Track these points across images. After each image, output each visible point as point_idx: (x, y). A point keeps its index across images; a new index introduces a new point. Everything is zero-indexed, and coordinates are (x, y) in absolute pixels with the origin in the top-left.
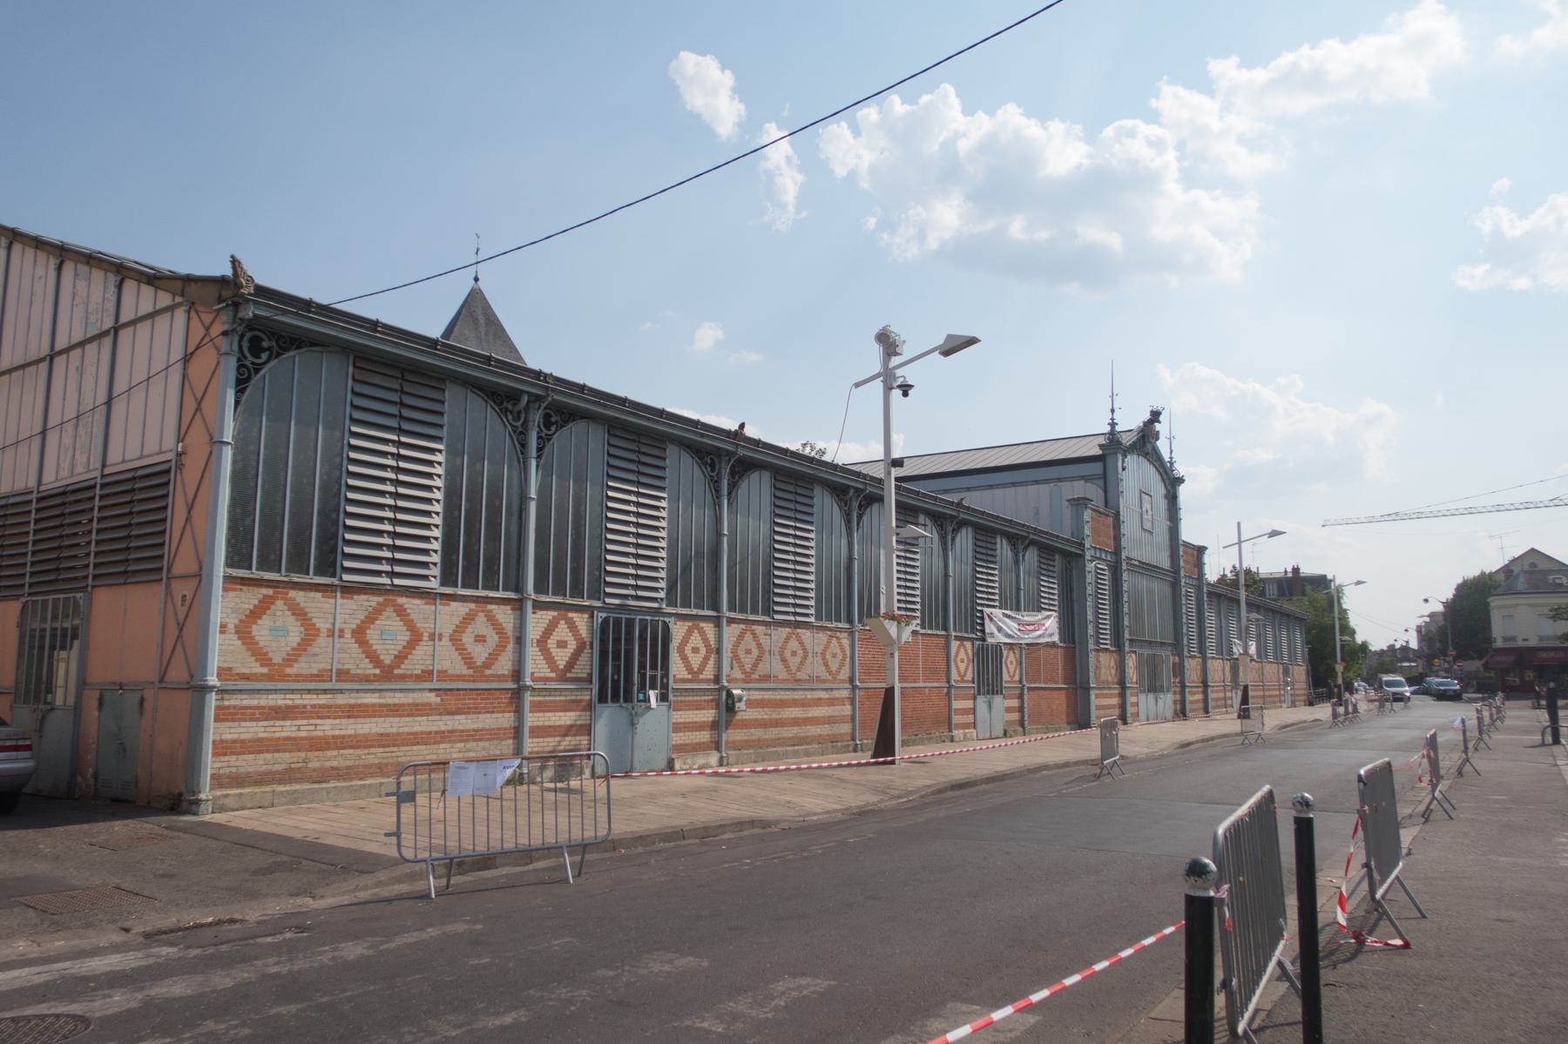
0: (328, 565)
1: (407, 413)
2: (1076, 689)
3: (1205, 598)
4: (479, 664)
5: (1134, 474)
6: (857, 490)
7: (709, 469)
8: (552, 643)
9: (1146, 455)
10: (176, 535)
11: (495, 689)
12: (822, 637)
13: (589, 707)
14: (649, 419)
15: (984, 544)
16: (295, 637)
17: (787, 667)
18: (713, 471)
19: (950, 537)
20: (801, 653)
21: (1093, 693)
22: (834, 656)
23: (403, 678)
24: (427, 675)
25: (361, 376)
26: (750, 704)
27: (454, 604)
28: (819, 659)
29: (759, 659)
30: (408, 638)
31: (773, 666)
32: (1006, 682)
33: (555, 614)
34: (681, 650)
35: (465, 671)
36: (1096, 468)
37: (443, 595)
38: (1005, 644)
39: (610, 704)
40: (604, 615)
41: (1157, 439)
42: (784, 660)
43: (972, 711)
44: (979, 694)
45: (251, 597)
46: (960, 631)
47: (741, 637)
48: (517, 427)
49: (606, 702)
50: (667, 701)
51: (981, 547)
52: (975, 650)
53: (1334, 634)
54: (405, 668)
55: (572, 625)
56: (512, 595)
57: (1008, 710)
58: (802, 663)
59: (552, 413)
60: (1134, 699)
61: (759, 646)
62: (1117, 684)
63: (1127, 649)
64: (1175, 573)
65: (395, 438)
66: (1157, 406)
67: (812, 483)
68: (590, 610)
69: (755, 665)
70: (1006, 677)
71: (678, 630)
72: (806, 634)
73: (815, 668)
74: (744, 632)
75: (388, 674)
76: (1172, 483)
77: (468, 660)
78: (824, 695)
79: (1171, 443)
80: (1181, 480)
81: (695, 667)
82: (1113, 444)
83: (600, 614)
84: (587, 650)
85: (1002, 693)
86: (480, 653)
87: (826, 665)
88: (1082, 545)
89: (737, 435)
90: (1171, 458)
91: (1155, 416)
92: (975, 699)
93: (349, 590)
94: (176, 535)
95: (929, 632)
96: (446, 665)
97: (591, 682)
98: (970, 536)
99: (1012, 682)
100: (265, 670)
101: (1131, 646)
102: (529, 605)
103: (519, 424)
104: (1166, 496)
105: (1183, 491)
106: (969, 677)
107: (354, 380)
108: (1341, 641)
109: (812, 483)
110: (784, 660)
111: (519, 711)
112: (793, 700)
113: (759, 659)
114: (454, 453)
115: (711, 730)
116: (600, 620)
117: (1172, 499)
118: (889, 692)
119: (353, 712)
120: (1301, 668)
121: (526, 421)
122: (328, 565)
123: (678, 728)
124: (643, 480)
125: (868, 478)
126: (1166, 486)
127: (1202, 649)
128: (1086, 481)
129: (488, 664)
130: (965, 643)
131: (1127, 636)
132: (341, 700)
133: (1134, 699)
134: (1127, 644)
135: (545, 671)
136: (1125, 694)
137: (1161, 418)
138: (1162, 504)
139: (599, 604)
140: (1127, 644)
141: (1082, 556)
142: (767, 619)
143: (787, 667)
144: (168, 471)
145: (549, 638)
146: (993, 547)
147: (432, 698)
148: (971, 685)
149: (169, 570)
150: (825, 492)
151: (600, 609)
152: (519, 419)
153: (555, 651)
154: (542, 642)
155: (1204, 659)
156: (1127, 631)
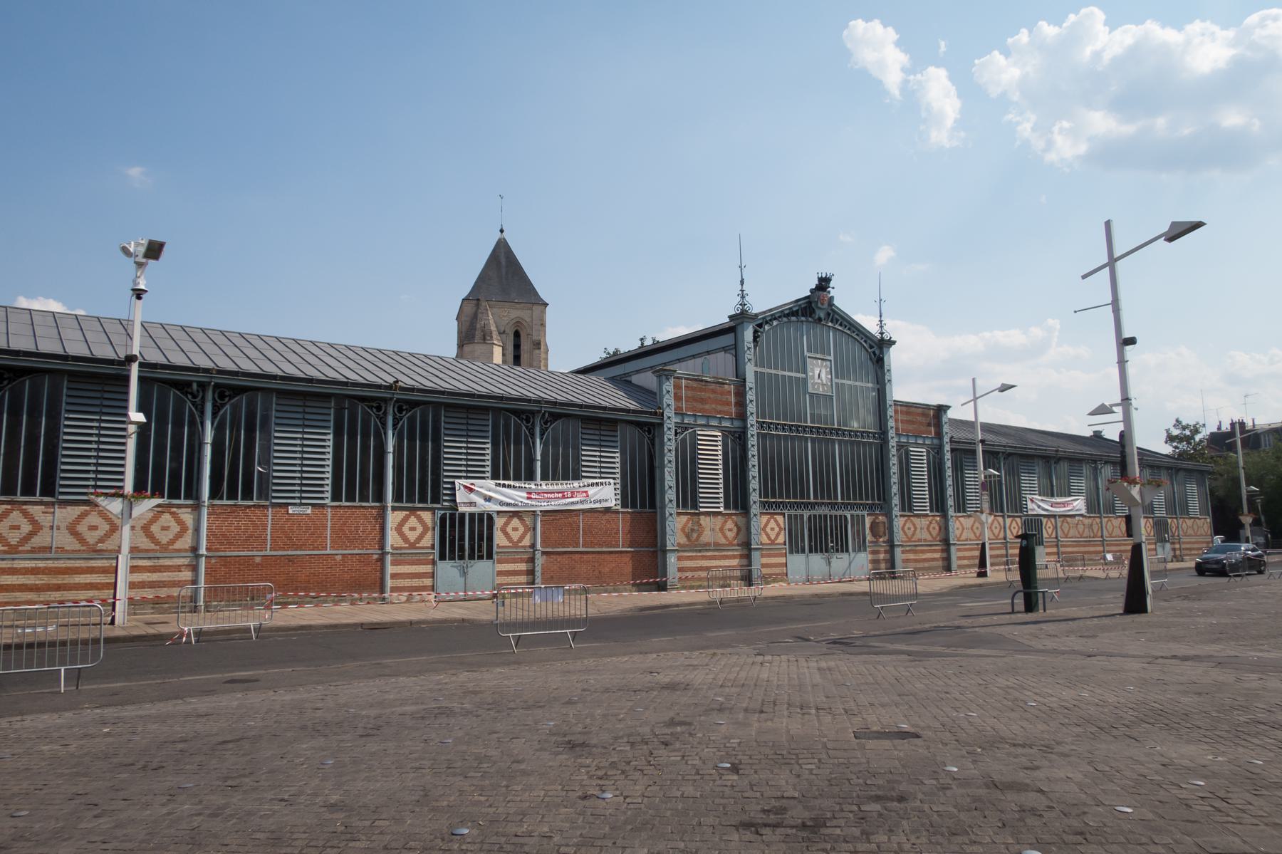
0: (49, 490)
1: (470, 428)
2: (655, 552)
4: (515, 541)
6: (1003, 452)
7: (647, 433)
11: (357, 554)
13: (434, 563)
14: (508, 404)
18: (649, 434)
25: (448, 414)
27: (69, 508)
30: (152, 527)
32: (1046, 538)
33: (408, 513)
35: (975, 538)
38: (499, 512)
39: (819, 553)
40: (442, 512)
43: (431, 575)
44: (442, 557)
45: (403, 514)
46: (1146, 514)
48: (379, 415)
49: (445, 559)
50: (492, 558)
52: (1023, 522)
55: (776, 521)
56: (190, 502)
59: (225, 390)
62: (940, 541)
65: (98, 417)
68: (433, 510)
70: (1045, 535)
77: (406, 539)
83: (439, 512)
84: (783, 532)
85: (1043, 545)
86: (412, 536)
89: (392, 387)
92: (434, 563)
93: (969, 516)
97: (785, 545)
98: (1066, 465)
99: (1050, 537)
100: (511, 544)
103: (651, 436)
106: (1152, 534)
107: (582, 428)
108: (1247, 492)
111: (1006, 549)
112: (88, 567)
114: (623, 454)
115: (527, 575)
116: (439, 515)
118: (983, 545)
121: (533, 422)
122: (49, 490)
123: (500, 573)
124: (105, 410)
125: (214, 372)
129: (998, 535)
135: (401, 543)
136: (950, 549)
139: (439, 506)
145: (403, 526)
146: (1081, 472)
148: (783, 547)
151: (439, 509)
152: (381, 410)
153: (976, 531)
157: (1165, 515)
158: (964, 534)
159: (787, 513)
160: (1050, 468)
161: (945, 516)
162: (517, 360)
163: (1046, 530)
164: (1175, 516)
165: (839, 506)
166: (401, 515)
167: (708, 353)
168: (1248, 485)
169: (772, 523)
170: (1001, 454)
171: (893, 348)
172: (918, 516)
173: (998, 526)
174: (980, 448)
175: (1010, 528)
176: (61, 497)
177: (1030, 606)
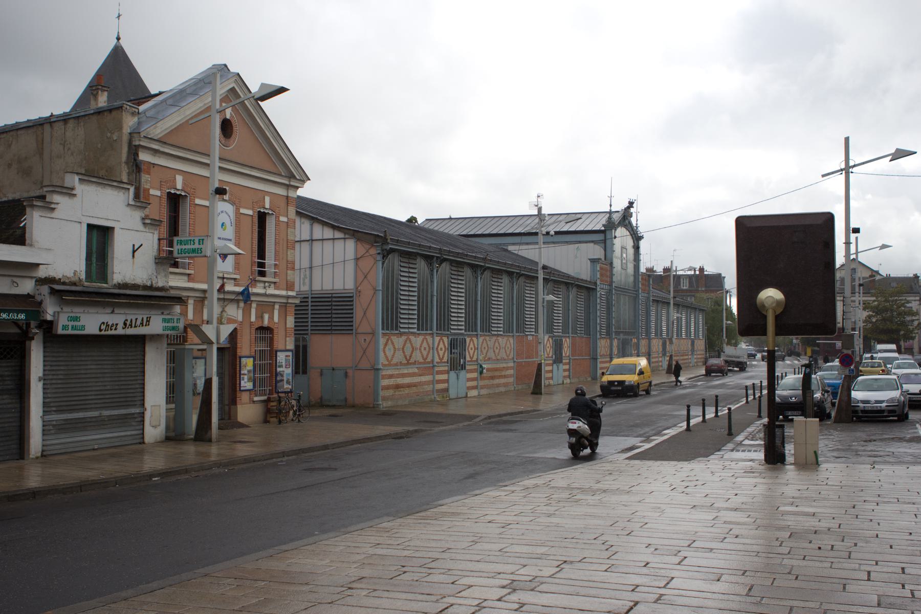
5: (621, 237)
9: (625, 226)
15: (456, 273)
19: (435, 271)
21: (599, 360)
28: (504, 350)
32: (468, 361)
36: (600, 237)
37: (418, 334)
41: (631, 217)
44: (451, 370)
51: (455, 275)
52: (449, 341)
57: (565, 370)
63: (614, 337)
64: (636, 291)
66: (633, 198)
67: (416, 256)
71: (468, 340)
72: (500, 339)
75: (408, 363)
76: (637, 238)
78: (505, 365)
79: (640, 219)
80: (641, 238)
82: (610, 226)
88: (595, 284)
90: (637, 224)
91: (631, 204)
92: (552, 366)
93: (401, 334)
95: (440, 332)
99: (549, 357)
101: (615, 335)
104: (634, 247)
105: (642, 243)
109: (416, 256)
117: (637, 248)
119: (403, 376)
120: (702, 341)
126: (634, 242)
127: (648, 333)
128: (595, 243)
130: (410, 337)
131: (614, 330)
134: (613, 334)
137: (634, 205)
138: (631, 251)
140: (613, 334)
141: (596, 289)
142: (490, 334)
144: (352, 297)
147: (416, 370)
148: (446, 364)
149: (356, 330)
150: (422, 260)
155: (649, 339)
156: (613, 328)
157: (463, 332)
160: (477, 278)
162: (209, 155)
163: (445, 347)
164: (429, 332)
167: (580, 242)
168: (727, 320)
170: (435, 258)
171: (725, 279)
173: (427, 346)
174: (541, 276)
175: (437, 349)
176: (402, 330)
177: (704, 400)
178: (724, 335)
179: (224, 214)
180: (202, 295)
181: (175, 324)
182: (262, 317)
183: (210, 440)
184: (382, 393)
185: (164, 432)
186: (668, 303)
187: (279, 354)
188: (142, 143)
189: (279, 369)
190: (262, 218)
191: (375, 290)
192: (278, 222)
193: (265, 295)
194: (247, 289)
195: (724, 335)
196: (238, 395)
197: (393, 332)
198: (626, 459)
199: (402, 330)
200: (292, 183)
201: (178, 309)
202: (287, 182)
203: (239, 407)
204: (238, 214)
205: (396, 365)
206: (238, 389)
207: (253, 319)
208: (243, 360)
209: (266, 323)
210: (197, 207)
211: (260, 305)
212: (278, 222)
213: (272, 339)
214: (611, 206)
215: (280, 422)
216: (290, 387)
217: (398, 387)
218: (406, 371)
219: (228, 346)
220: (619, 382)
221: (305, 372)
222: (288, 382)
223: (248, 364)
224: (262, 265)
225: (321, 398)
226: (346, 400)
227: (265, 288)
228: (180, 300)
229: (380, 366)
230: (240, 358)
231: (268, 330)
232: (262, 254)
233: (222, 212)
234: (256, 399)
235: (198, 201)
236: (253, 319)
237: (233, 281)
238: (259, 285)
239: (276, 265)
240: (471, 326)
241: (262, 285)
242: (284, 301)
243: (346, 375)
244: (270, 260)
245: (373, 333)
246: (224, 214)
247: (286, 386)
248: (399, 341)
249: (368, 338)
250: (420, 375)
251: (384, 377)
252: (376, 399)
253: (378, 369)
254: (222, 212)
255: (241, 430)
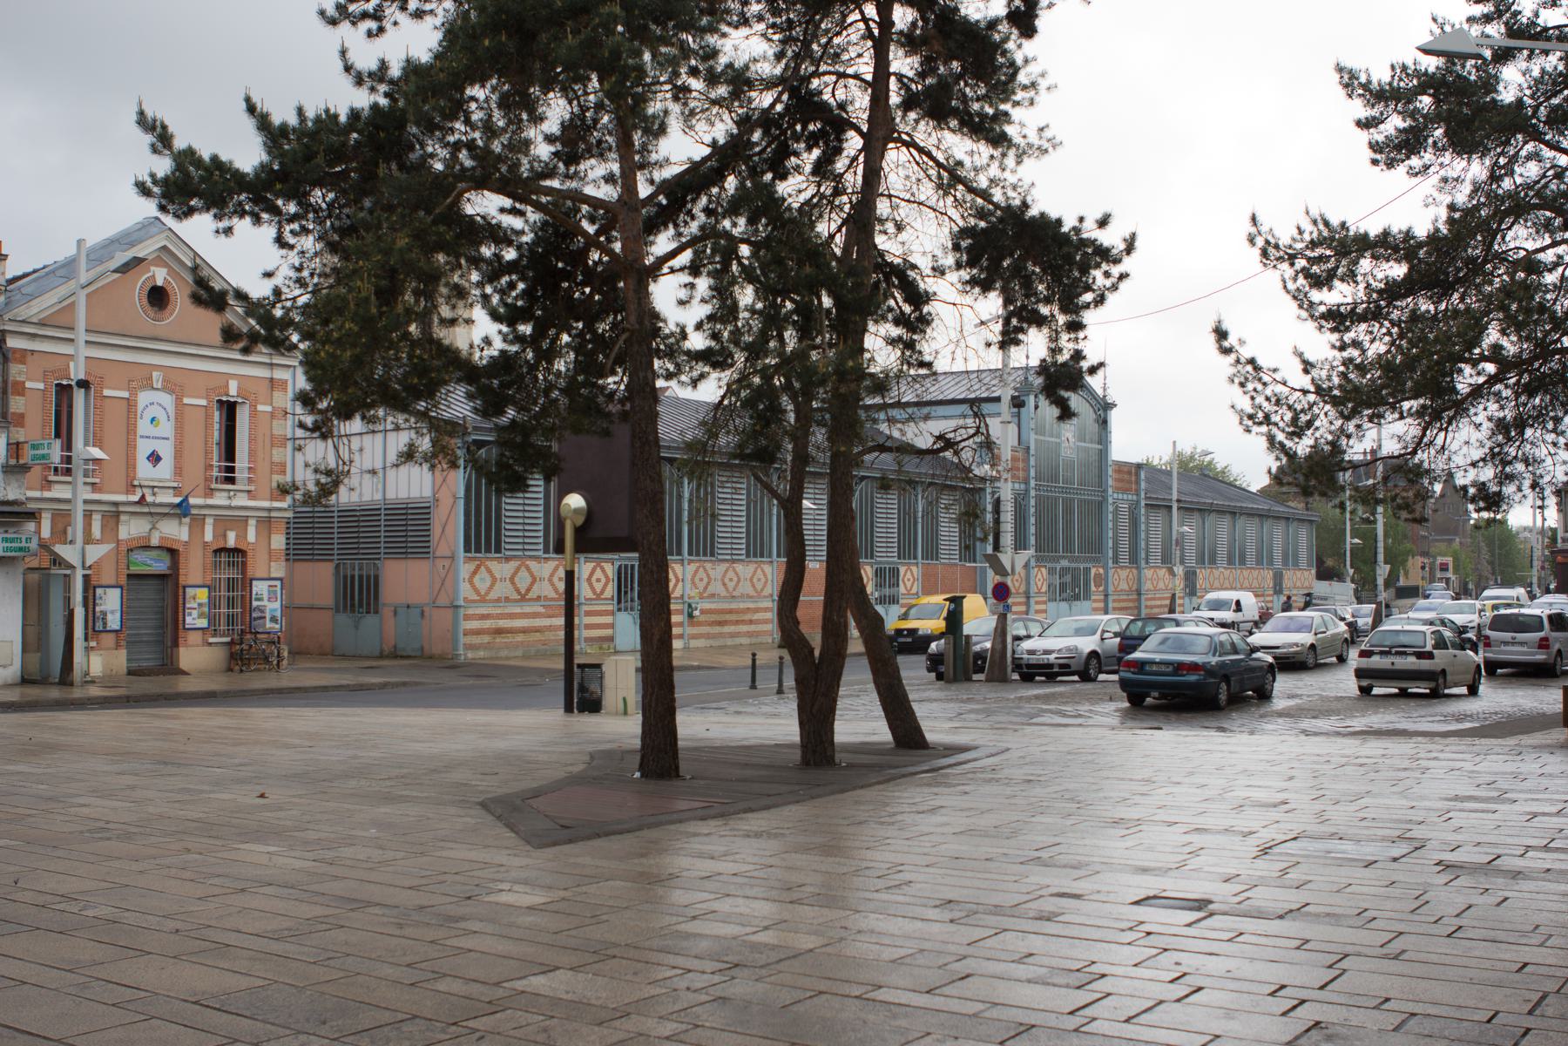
0: (498, 550)
3: (1143, 511)
8: (594, 579)
10: (436, 538)
12: (752, 567)
16: (488, 583)
17: (727, 589)
20: (755, 580)
22: (759, 580)
23: (530, 600)
24: (539, 598)
26: (702, 612)
28: (720, 583)
29: (708, 583)
31: (716, 588)
34: (589, 580)
42: (724, 584)
47: (696, 572)
53: (1345, 535)
54: (530, 595)
55: (603, 571)
58: (737, 585)
60: (1181, 601)
61: (708, 575)
69: (706, 588)
71: (902, 570)
73: (746, 588)
74: (698, 568)
75: (523, 598)
78: (751, 605)
81: (598, 591)
87: (754, 586)
93: (508, 559)
94: (436, 538)
96: (546, 593)
102: (686, 562)
110: (724, 584)
113: (708, 583)
119: (512, 616)
129: (602, 591)
132: (507, 611)
133: (1181, 601)
143: (727, 589)
147: (542, 610)
154: (589, 580)
158: (535, 587)
159: (1048, 565)
161: (1138, 568)
165: (1077, 560)
166: (472, 566)
169: (598, 574)
172: (1122, 567)
176: (508, 553)
178: (1348, 563)
179: (155, 406)
180: (114, 509)
181: (24, 544)
182: (225, 536)
183: (72, 684)
184: (463, 640)
185: (19, 673)
186: (1171, 507)
187: (254, 583)
188: (6, 328)
189: (255, 604)
190: (229, 409)
191: (455, 498)
192: (254, 413)
193: (230, 508)
194: (186, 499)
195: (1348, 563)
196: (181, 634)
197: (488, 555)
198: (976, 748)
199: (508, 553)
200: (274, 361)
201: (31, 526)
202: (268, 361)
203: (182, 650)
204: (180, 407)
205: (498, 600)
206: (181, 627)
207: (209, 536)
208: (190, 592)
209: (231, 540)
210: (108, 400)
211: (218, 520)
212: (254, 413)
213: (244, 564)
214: (1027, 357)
215: (242, 671)
216: (278, 626)
217: (499, 631)
218: (518, 610)
219: (168, 572)
220: (908, 630)
221: (376, 612)
222: (274, 619)
223: (198, 597)
224: (231, 470)
225: (395, 647)
226: (422, 649)
227: (230, 498)
228: (32, 515)
229: (461, 603)
230: (184, 587)
231: (237, 555)
232: (229, 452)
233: (152, 404)
234: (212, 640)
235: (107, 392)
236: (209, 536)
237: (171, 491)
238: (217, 494)
239: (250, 468)
240: (906, 551)
241: (225, 494)
242: (265, 514)
243: (422, 613)
244: (242, 462)
245: (452, 558)
246: (155, 406)
247: (269, 625)
248: (502, 569)
249: (447, 563)
250: (550, 617)
251: (467, 618)
252: (455, 648)
253: (457, 607)
254: (152, 404)
255: (184, 678)
